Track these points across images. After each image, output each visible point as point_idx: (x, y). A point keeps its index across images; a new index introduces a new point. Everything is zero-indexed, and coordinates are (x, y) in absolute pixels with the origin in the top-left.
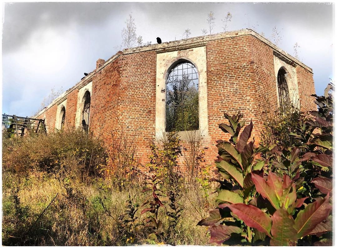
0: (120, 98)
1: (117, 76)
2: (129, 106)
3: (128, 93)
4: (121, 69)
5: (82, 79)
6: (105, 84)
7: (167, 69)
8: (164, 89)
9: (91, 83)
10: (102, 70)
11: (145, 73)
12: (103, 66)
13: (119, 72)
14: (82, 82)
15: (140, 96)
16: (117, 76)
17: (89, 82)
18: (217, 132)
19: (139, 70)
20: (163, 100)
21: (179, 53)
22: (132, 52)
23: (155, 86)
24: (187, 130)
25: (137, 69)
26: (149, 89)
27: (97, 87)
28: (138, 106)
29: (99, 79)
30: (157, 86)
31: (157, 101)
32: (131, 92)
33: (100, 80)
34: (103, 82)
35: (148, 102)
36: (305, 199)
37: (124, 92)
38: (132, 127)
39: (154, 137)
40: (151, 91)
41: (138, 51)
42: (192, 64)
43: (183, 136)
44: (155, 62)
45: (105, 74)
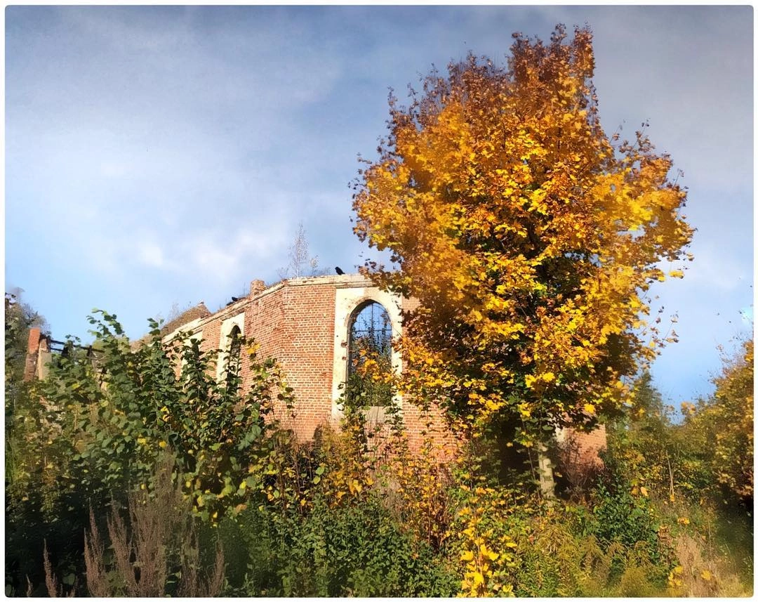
0: (283, 350)
1: (281, 317)
2: (296, 364)
3: (295, 344)
4: (286, 307)
5: (228, 305)
6: (263, 323)
7: (350, 313)
8: (345, 341)
9: (242, 315)
10: (259, 300)
11: (319, 316)
12: (261, 295)
13: (283, 312)
14: (229, 310)
15: (312, 351)
16: (281, 317)
17: (240, 312)
18: (412, 412)
19: (311, 311)
20: (343, 358)
21: (367, 291)
22: (302, 283)
23: (332, 336)
24: (377, 405)
25: (309, 309)
26: (324, 340)
27: (252, 325)
28: (309, 365)
29: (255, 313)
30: (335, 336)
31: (335, 359)
32: (300, 344)
33: (257, 315)
34: (261, 321)
35: (323, 360)
36: (12, 328)
37: (289, 342)
38: (299, 395)
39: (329, 412)
40: (326, 344)
41: (310, 283)
42: (351, 334)
43: (374, 414)
44: (333, 302)
45: (263, 307)
